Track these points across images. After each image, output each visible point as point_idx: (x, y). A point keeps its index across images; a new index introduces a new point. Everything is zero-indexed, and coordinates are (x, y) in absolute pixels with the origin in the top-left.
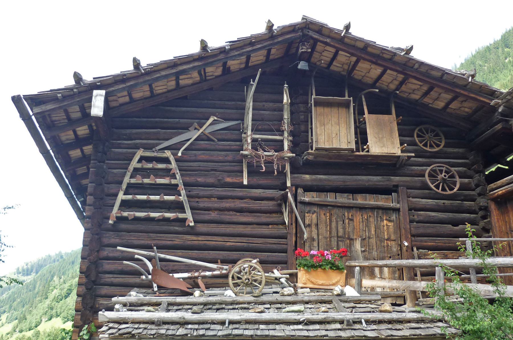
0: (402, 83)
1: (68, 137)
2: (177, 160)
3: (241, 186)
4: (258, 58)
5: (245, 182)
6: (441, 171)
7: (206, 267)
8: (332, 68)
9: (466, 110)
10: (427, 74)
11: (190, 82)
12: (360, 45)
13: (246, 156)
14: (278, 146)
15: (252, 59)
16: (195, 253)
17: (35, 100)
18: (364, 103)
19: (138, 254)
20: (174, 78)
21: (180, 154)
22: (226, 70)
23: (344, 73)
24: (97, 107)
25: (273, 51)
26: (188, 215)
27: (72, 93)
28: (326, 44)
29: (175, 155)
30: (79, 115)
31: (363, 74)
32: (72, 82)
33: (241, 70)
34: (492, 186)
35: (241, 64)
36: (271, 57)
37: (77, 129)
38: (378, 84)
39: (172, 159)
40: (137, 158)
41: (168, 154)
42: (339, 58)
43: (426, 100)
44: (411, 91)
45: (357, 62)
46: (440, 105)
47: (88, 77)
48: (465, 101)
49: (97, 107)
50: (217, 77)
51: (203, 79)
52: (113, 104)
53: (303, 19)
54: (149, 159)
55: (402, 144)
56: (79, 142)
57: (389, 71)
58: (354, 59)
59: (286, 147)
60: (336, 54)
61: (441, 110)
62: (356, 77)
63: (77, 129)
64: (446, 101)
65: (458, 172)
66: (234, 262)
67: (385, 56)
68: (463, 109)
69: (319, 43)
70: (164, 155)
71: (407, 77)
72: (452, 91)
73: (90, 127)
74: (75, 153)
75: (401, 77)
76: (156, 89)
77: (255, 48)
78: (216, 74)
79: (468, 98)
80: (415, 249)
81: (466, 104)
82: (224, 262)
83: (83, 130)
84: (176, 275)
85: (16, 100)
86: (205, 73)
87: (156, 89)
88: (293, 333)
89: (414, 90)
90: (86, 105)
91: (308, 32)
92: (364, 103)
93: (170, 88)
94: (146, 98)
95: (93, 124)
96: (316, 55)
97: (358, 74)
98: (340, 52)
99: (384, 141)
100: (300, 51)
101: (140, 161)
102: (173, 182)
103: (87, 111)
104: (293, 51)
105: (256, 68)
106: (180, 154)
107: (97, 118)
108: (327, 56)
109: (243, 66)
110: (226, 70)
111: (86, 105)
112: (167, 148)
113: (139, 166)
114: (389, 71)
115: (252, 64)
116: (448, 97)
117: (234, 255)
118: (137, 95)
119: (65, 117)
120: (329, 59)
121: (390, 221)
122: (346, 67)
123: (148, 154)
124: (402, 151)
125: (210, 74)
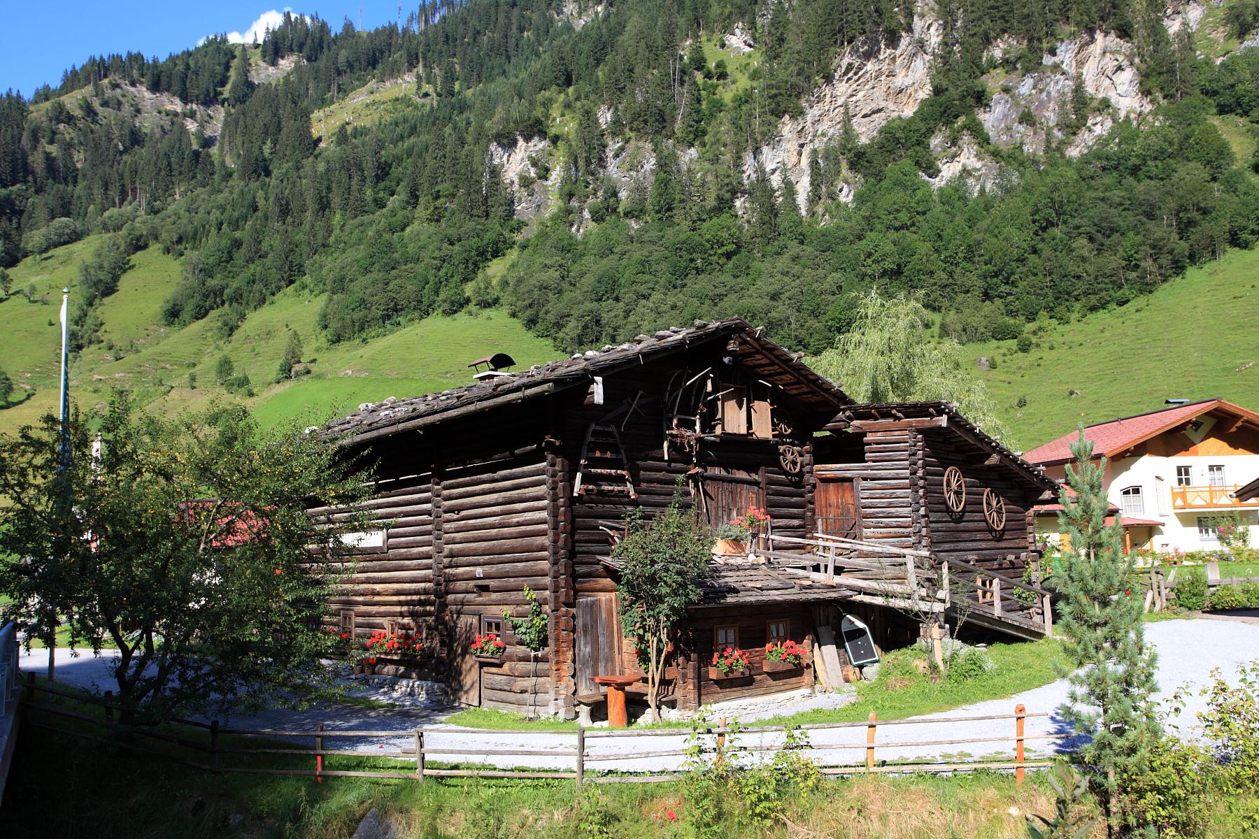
24: (598, 393)
41: (612, 428)
49: (598, 393)
124: (774, 436)
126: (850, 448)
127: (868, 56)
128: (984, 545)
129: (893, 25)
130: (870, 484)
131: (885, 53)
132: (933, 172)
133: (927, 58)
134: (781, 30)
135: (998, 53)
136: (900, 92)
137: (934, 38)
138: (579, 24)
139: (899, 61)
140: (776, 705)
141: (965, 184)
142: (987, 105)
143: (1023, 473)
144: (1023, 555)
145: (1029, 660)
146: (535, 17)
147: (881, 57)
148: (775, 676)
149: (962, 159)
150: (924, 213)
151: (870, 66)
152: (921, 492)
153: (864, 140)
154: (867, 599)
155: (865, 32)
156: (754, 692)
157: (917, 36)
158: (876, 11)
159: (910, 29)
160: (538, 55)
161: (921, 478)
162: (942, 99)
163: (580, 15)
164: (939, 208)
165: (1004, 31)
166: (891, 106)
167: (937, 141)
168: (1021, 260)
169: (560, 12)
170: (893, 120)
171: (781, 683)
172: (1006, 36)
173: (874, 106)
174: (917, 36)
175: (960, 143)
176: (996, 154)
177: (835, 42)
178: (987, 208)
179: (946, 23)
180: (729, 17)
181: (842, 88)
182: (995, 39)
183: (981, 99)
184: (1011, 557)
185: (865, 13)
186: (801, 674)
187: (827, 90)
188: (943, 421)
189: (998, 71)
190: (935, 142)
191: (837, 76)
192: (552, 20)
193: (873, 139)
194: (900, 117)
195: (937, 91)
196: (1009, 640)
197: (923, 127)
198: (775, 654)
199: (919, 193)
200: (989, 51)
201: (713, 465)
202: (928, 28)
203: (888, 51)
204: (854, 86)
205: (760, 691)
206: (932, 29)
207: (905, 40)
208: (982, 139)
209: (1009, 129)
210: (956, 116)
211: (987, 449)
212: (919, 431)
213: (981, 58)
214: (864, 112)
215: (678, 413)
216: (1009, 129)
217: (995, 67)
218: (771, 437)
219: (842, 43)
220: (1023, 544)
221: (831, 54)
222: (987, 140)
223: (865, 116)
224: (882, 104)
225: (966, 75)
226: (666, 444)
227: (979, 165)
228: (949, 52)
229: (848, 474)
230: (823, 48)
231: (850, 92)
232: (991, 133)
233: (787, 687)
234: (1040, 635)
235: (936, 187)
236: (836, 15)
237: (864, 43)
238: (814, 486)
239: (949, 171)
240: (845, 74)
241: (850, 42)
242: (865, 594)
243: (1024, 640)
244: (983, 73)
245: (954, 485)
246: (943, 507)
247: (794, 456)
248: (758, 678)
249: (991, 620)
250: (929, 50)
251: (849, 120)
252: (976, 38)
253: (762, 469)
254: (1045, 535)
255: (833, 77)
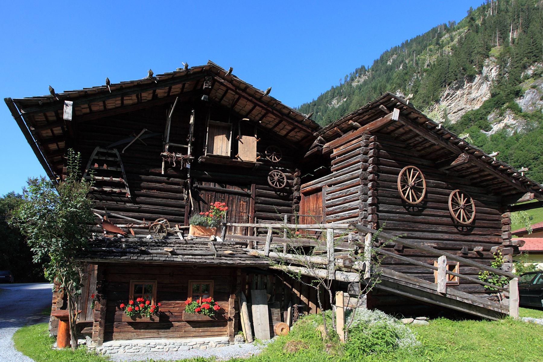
0: (264, 116)
1: (48, 134)
2: (122, 155)
3: (160, 174)
4: (176, 88)
5: (163, 173)
6: (277, 175)
7: (134, 222)
8: (223, 102)
9: (298, 138)
10: (280, 111)
11: (130, 102)
12: (242, 86)
13: (164, 156)
14: (185, 151)
15: (172, 90)
16: (131, 214)
17: (23, 104)
18: (239, 128)
19: (97, 212)
20: (120, 98)
21: (123, 152)
22: (155, 96)
23: (229, 107)
24: (68, 113)
25: (186, 85)
26: (127, 190)
27: (49, 101)
28: (222, 84)
29: (120, 152)
30: (55, 118)
31: (241, 108)
32: (48, 94)
33: (165, 97)
34: (304, 185)
35: (165, 93)
36: (185, 90)
37: (54, 129)
38: (249, 116)
39: (118, 154)
40: (95, 152)
41: (115, 151)
42: (228, 95)
43: (276, 129)
44: (268, 122)
45: (238, 99)
46: (284, 133)
47: (59, 91)
48: (299, 132)
49: (68, 113)
50: (149, 101)
51: (139, 100)
52: (78, 113)
53: (209, 63)
54: (103, 154)
55: (257, 156)
56: (55, 139)
57: (257, 107)
58: (237, 96)
59: (189, 153)
60: (226, 92)
61: (283, 136)
62: (236, 110)
63: (54, 129)
64: (287, 131)
65: (286, 176)
66: (154, 220)
67: (256, 96)
68: (296, 137)
69: (216, 83)
70: (114, 152)
71: (268, 112)
72: (293, 124)
73: (63, 129)
74: (53, 147)
75: (264, 112)
76: (108, 105)
77: (175, 81)
78: (148, 99)
79: (301, 129)
80: (256, 219)
81: (299, 134)
82: (147, 219)
83: (58, 130)
84: (118, 226)
85: (10, 102)
86: (141, 97)
87: (108, 105)
88: (187, 260)
89: (271, 120)
90: (60, 111)
91: (211, 72)
92: (239, 128)
93: (117, 106)
94: (100, 111)
95: (65, 126)
96: (213, 92)
97: (237, 108)
98: (229, 91)
99: (249, 150)
100: (204, 87)
101: (97, 155)
102: (119, 170)
103: (61, 116)
104: (199, 87)
105: (174, 97)
106: (123, 152)
107: (67, 121)
108: (220, 93)
109: (166, 95)
110: (155, 96)
111: (60, 111)
112: (115, 147)
113: (97, 158)
114: (257, 107)
115: (173, 94)
116: (289, 128)
117: (154, 216)
118: (95, 108)
119: (45, 119)
120: (221, 96)
121: (244, 202)
122: (231, 102)
123: (102, 150)
124: (257, 160)
125: (144, 98)
126: (321, 165)
127: (457, 89)
128: (446, 236)
129: (472, 73)
130: (333, 188)
131: (467, 85)
132: (488, 128)
133: (489, 83)
134: (417, 88)
135: (530, 72)
136: (473, 100)
137: (494, 74)
138: (337, 106)
139: (473, 88)
140: (186, 348)
141: (506, 131)
142: (521, 96)
143: (501, 178)
144: (494, 248)
145: (475, 340)
146: (322, 107)
147: (464, 88)
148: (195, 324)
149: (505, 121)
150: (482, 146)
151: (458, 92)
152: (370, 185)
153: (453, 122)
154: (284, 268)
155: (457, 79)
156: (171, 334)
157: (484, 75)
158: (463, 69)
159: (480, 73)
160: (322, 119)
161: (371, 173)
162: (495, 98)
163: (338, 103)
164: (490, 143)
165: (535, 62)
166: (468, 106)
167: (491, 116)
168: (536, 159)
169: (331, 104)
170: (469, 112)
171: (201, 330)
172: (536, 63)
173: (459, 108)
174: (484, 75)
175: (504, 115)
176: (525, 116)
177: (442, 87)
178: (517, 140)
179: (501, 66)
180: (394, 89)
181: (444, 104)
182: (529, 66)
183: (518, 94)
184: (480, 248)
185: (457, 71)
186: (225, 325)
187: (436, 106)
188: (395, 115)
189: (529, 80)
190: (490, 117)
191: (441, 99)
192: (328, 107)
193: (457, 121)
194: (472, 110)
195: (493, 95)
196: (456, 316)
197: (484, 112)
198: (190, 307)
199: (480, 139)
200: (525, 72)
201: (208, 180)
202: (491, 70)
203: (468, 84)
204: (450, 102)
205: (176, 334)
206: (493, 71)
207: (478, 78)
208: (516, 110)
209: (534, 104)
210: (503, 104)
211: (453, 148)
212: (372, 133)
213: (520, 76)
214: (454, 111)
215: (171, 141)
216: (534, 104)
217: (528, 79)
218: (255, 160)
219: (445, 86)
220: (496, 239)
221: (439, 91)
222: (520, 111)
223: (454, 113)
224: (463, 106)
225: (511, 85)
226: (163, 163)
227: (515, 122)
228: (502, 78)
229: (319, 185)
230: (436, 90)
231: (447, 104)
232: (522, 108)
233: (207, 333)
234: (502, 316)
235: (489, 135)
236: (443, 76)
237: (456, 84)
238: (299, 198)
239: (496, 128)
240: (445, 98)
241: (449, 85)
242: (293, 265)
243: (480, 319)
244: (520, 83)
245: (411, 182)
246: (398, 201)
247: (278, 176)
248: (176, 324)
249: (432, 295)
250: (490, 79)
251: (446, 116)
252: (517, 68)
253: (253, 186)
254: (534, 264)
255: (440, 100)
